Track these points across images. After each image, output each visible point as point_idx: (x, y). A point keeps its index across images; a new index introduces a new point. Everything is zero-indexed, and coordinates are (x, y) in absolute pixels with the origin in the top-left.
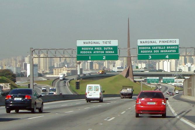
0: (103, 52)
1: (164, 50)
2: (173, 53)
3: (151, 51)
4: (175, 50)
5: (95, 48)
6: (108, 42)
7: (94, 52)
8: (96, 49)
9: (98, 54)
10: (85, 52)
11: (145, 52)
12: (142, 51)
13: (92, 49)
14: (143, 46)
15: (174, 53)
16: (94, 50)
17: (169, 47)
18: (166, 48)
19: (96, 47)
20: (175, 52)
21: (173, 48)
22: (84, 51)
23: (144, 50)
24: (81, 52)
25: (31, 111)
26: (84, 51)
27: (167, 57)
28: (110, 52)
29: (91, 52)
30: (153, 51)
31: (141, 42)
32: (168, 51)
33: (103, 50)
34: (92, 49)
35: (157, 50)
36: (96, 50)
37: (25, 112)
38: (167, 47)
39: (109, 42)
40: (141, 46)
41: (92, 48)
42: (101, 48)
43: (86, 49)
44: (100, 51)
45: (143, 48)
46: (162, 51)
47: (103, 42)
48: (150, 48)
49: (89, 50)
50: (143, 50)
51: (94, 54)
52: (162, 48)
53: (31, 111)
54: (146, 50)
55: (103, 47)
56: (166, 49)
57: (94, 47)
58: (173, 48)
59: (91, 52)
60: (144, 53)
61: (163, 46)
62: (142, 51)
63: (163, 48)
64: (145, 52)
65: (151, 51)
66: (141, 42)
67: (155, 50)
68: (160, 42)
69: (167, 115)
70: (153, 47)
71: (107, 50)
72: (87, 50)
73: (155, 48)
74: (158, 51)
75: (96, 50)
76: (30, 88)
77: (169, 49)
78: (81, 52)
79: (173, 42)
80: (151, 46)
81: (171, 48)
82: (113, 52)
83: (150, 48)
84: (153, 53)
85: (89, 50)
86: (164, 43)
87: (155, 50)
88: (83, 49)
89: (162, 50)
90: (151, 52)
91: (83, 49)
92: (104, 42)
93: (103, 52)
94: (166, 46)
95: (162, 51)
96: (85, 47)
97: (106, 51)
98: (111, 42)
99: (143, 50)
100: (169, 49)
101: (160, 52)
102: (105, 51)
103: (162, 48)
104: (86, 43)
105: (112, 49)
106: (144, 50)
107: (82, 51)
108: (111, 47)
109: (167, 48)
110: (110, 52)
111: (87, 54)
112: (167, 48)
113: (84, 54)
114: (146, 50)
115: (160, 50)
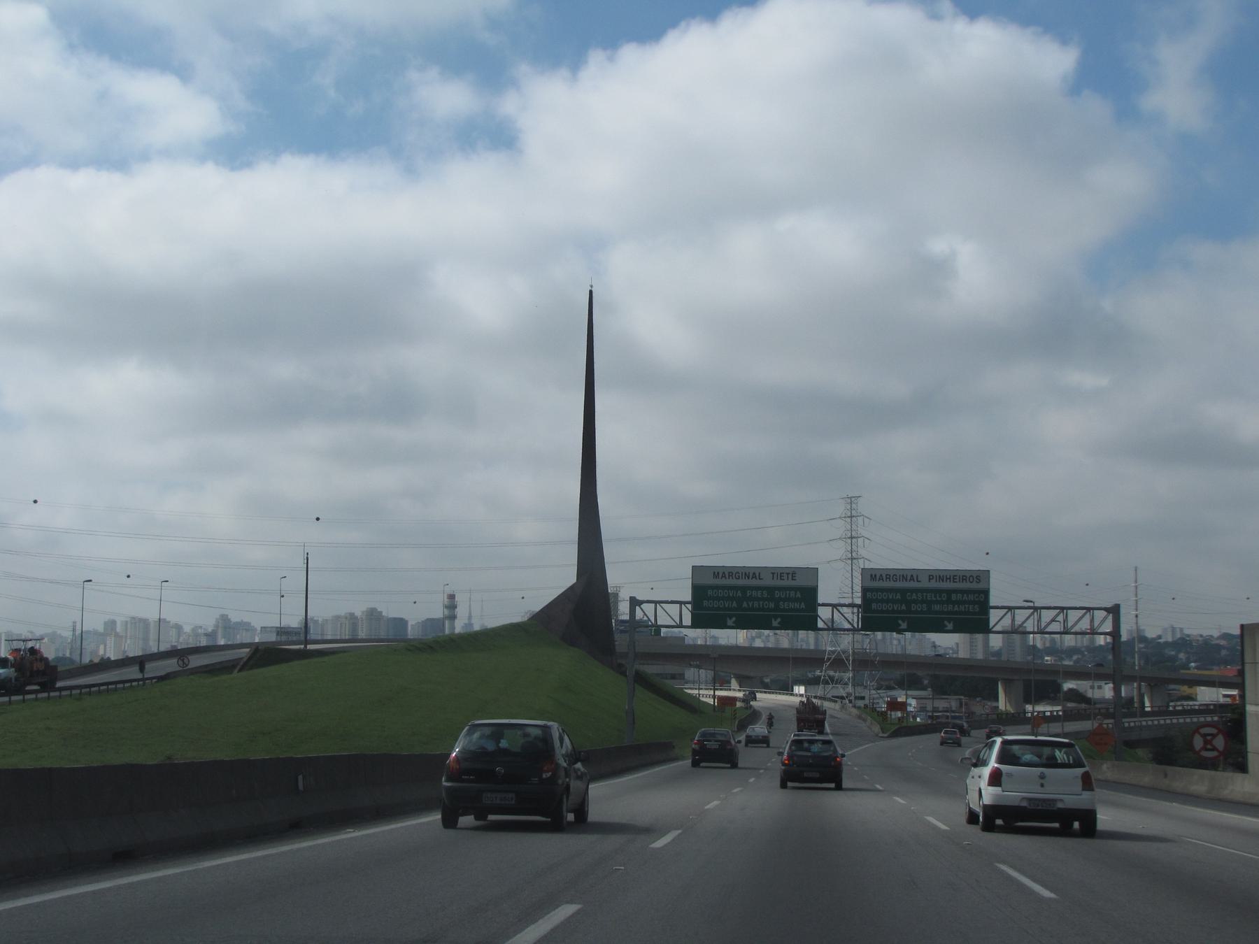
0: (772, 605)
4: (925, 605)
6: (788, 574)
7: (745, 605)
12: (874, 606)
13: (739, 594)
17: (959, 596)
19: (956, 591)
20: (977, 610)
23: (882, 601)
25: (729, 766)
27: (904, 626)
28: (792, 605)
29: (735, 604)
32: (956, 608)
34: (739, 594)
39: (790, 576)
41: (898, 594)
44: (761, 603)
46: (937, 607)
47: (773, 574)
48: (899, 596)
52: (935, 597)
53: (729, 766)
54: (888, 601)
55: (771, 590)
57: (744, 589)
58: (971, 597)
59: (735, 604)
60: (882, 612)
61: (940, 591)
62: (874, 606)
63: (940, 597)
64: (884, 607)
67: (915, 602)
68: (930, 579)
69: (844, 786)
70: (909, 594)
73: (914, 597)
74: (925, 605)
77: (959, 603)
79: (971, 579)
80: (903, 591)
81: (965, 597)
82: (803, 606)
83: (899, 596)
86: (944, 583)
90: (904, 607)
91: (710, 592)
92: (775, 576)
94: (950, 592)
95: (937, 607)
96: (717, 587)
100: (959, 603)
103: (935, 597)
104: (909, 578)
105: (799, 595)
106: (882, 601)
108: (796, 589)
109: (954, 597)
110: (792, 605)
111: (893, 611)
114: (888, 601)
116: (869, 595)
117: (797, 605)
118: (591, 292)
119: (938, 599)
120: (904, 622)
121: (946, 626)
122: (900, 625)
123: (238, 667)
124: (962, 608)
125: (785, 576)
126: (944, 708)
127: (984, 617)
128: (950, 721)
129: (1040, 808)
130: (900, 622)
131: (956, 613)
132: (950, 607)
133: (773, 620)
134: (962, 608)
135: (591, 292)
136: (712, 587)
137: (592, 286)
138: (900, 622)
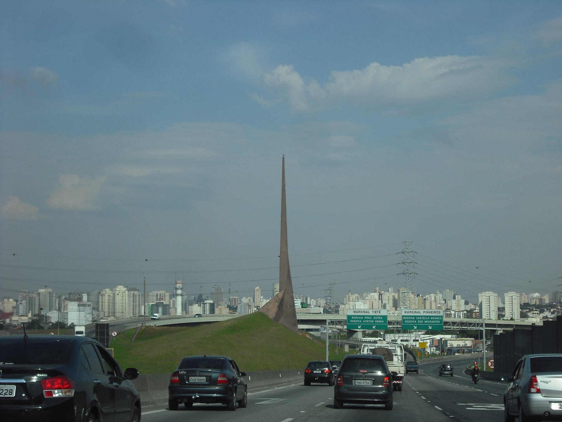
0: (373, 321)
1: (428, 320)
2: (436, 323)
3: (383, 321)
4: (370, 317)
5: (365, 318)
7: (364, 321)
8: (366, 318)
9: (368, 323)
10: (355, 321)
11: (409, 321)
12: (406, 321)
14: (407, 316)
15: (438, 323)
16: (364, 319)
18: (430, 318)
19: (432, 316)
21: (437, 318)
22: (354, 319)
23: (408, 320)
24: (351, 321)
26: (354, 319)
28: (379, 321)
29: (361, 321)
30: (417, 322)
31: (405, 312)
33: (373, 319)
34: (362, 318)
35: (421, 320)
36: (366, 319)
37: (319, 385)
38: (431, 318)
39: (379, 312)
40: (405, 316)
42: (370, 317)
43: (356, 318)
45: (407, 318)
46: (426, 322)
48: (414, 318)
49: (358, 319)
50: (407, 320)
51: (364, 323)
52: (426, 318)
54: (410, 320)
55: (372, 316)
56: (430, 320)
57: (364, 316)
58: (437, 318)
59: (361, 321)
60: (408, 323)
61: (427, 316)
62: (406, 321)
64: (409, 321)
65: (383, 321)
66: (405, 312)
67: (419, 320)
71: (377, 320)
72: (357, 319)
73: (419, 318)
74: (422, 321)
75: (366, 319)
76: (83, 332)
78: (351, 321)
80: (415, 317)
82: (383, 322)
84: (417, 323)
85: (358, 319)
87: (419, 320)
88: (353, 317)
89: (426, 320)
90: (415, 322)
93: (373, 321)
94: (430, 317)
95: (426, 322)
97: (376, 321)
98: (381, 312)
99: (407, 320)
101: (424, 323)
102: (374, 320)
103: (426, 318)
104: (366, 312)
105: (381, 318)
106: (408, 320)
107: (352, 319)
108: (380, 316)
110: (379, 321)
112: (431, 318)
113: (354, 323)
114: (410, 320)
115: (424, 320)
116: (404, 318)
117: (381, 322)
118: (283, 158)
119: (427, 319)
120: (415, 326)
121: (414, 328)
122: (414, 328)
123: (101, 345)
124: (434, 322)
125: (409, 312)
126: (463, 345)
127: (544, 320)
128: (403, 354)
129: (362, 384)
130: (429, 327)
131: (432, 323)
132: (431, 321)
133: (373, 326)
134: (434, 322)
135: (283, 158)
136: (354, 316)
137: (284, 155)
138: (414, 326)
